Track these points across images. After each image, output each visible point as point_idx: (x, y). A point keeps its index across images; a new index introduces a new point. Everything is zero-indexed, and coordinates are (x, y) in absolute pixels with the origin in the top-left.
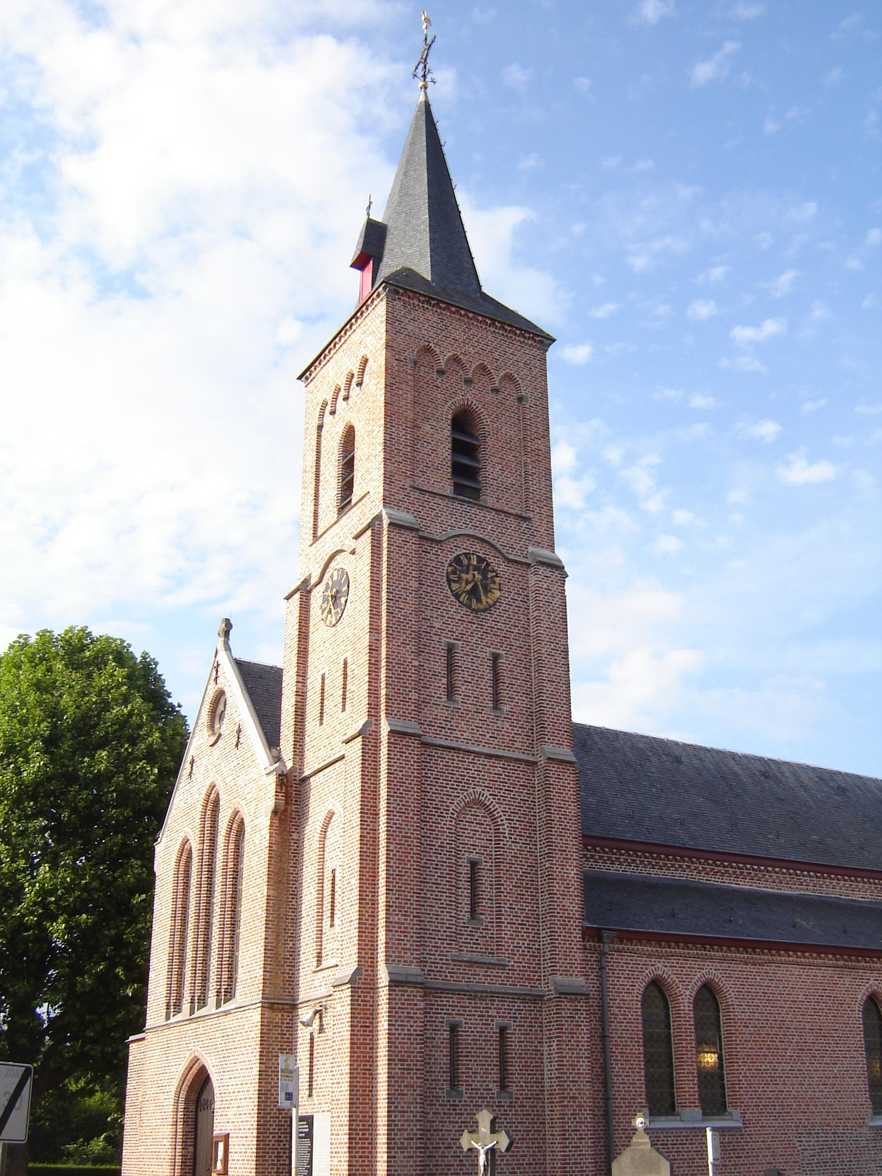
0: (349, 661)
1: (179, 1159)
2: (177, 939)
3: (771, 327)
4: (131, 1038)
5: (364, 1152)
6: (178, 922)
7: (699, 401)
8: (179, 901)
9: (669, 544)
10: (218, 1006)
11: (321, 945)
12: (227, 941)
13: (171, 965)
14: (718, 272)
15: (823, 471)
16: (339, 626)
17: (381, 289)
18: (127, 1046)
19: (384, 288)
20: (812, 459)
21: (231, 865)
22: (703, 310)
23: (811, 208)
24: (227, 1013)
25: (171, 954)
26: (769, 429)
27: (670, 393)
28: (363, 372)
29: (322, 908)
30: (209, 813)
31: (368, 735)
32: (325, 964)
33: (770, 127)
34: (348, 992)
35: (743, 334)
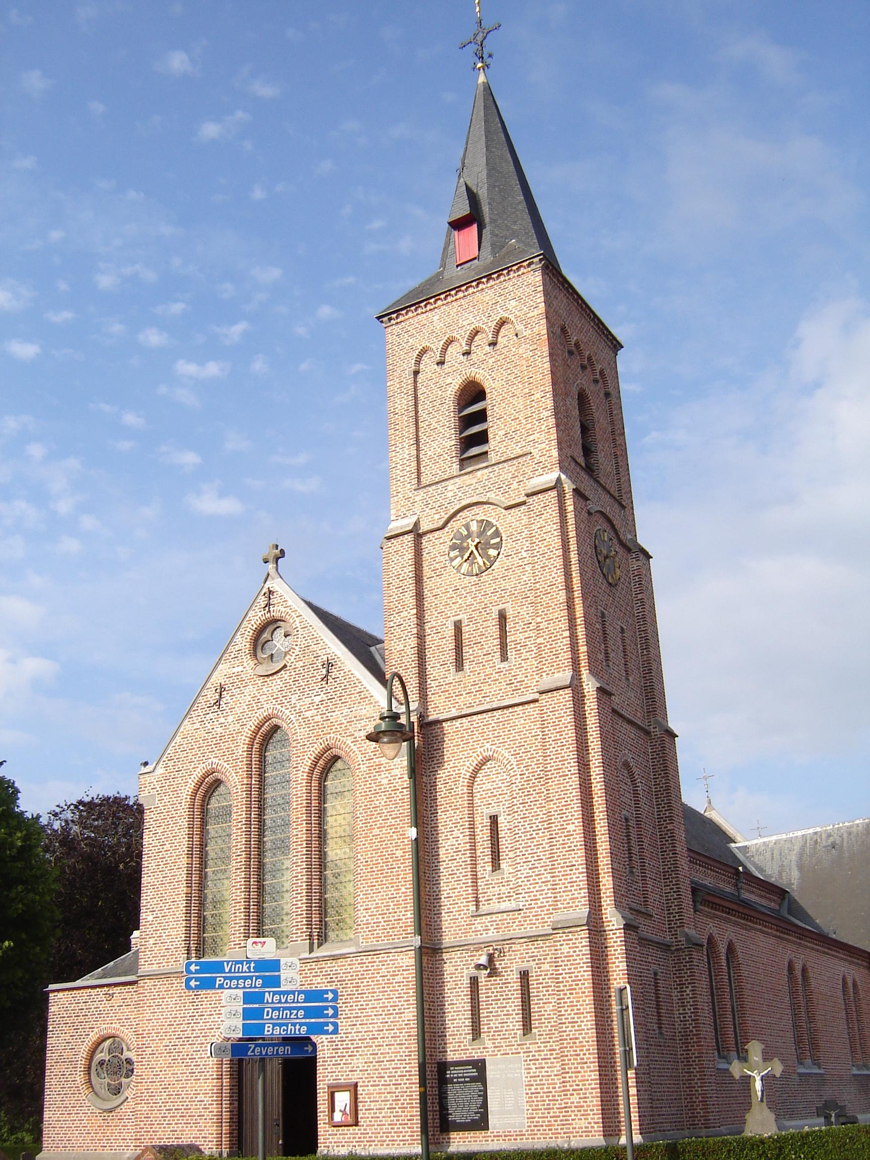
0: (510, 613)
1: (226, 1115)
2: (195, 878)
3: (213, 369)
4: (52, 987)
5: (566, 1095)
6: (196, 861)
7: (130, 419)
8: (196, 838)
9: (71, 545)
10: (311, 950)
11: (477, 890)
12: (315, 882)
13: (188, 906)
14: (178, 308)
15: (229, 506)
16: (484, 577)
17: (537, 259)
18: (46, 1000)
19: (541, 260)
20: (222, 494)
21: (315, 803)
22: (153, 338)
23: (274, 274)
24: (317, 960)
25: (189, 895)
26: (190, 458)
27: (106, 408)
28: (498, 333)
29: (475, 853)
30: (256, 746)
31: (575, 685)
32: (484, 908)
33: (258, 194)
34: (585, 934)
35: (186, 368)
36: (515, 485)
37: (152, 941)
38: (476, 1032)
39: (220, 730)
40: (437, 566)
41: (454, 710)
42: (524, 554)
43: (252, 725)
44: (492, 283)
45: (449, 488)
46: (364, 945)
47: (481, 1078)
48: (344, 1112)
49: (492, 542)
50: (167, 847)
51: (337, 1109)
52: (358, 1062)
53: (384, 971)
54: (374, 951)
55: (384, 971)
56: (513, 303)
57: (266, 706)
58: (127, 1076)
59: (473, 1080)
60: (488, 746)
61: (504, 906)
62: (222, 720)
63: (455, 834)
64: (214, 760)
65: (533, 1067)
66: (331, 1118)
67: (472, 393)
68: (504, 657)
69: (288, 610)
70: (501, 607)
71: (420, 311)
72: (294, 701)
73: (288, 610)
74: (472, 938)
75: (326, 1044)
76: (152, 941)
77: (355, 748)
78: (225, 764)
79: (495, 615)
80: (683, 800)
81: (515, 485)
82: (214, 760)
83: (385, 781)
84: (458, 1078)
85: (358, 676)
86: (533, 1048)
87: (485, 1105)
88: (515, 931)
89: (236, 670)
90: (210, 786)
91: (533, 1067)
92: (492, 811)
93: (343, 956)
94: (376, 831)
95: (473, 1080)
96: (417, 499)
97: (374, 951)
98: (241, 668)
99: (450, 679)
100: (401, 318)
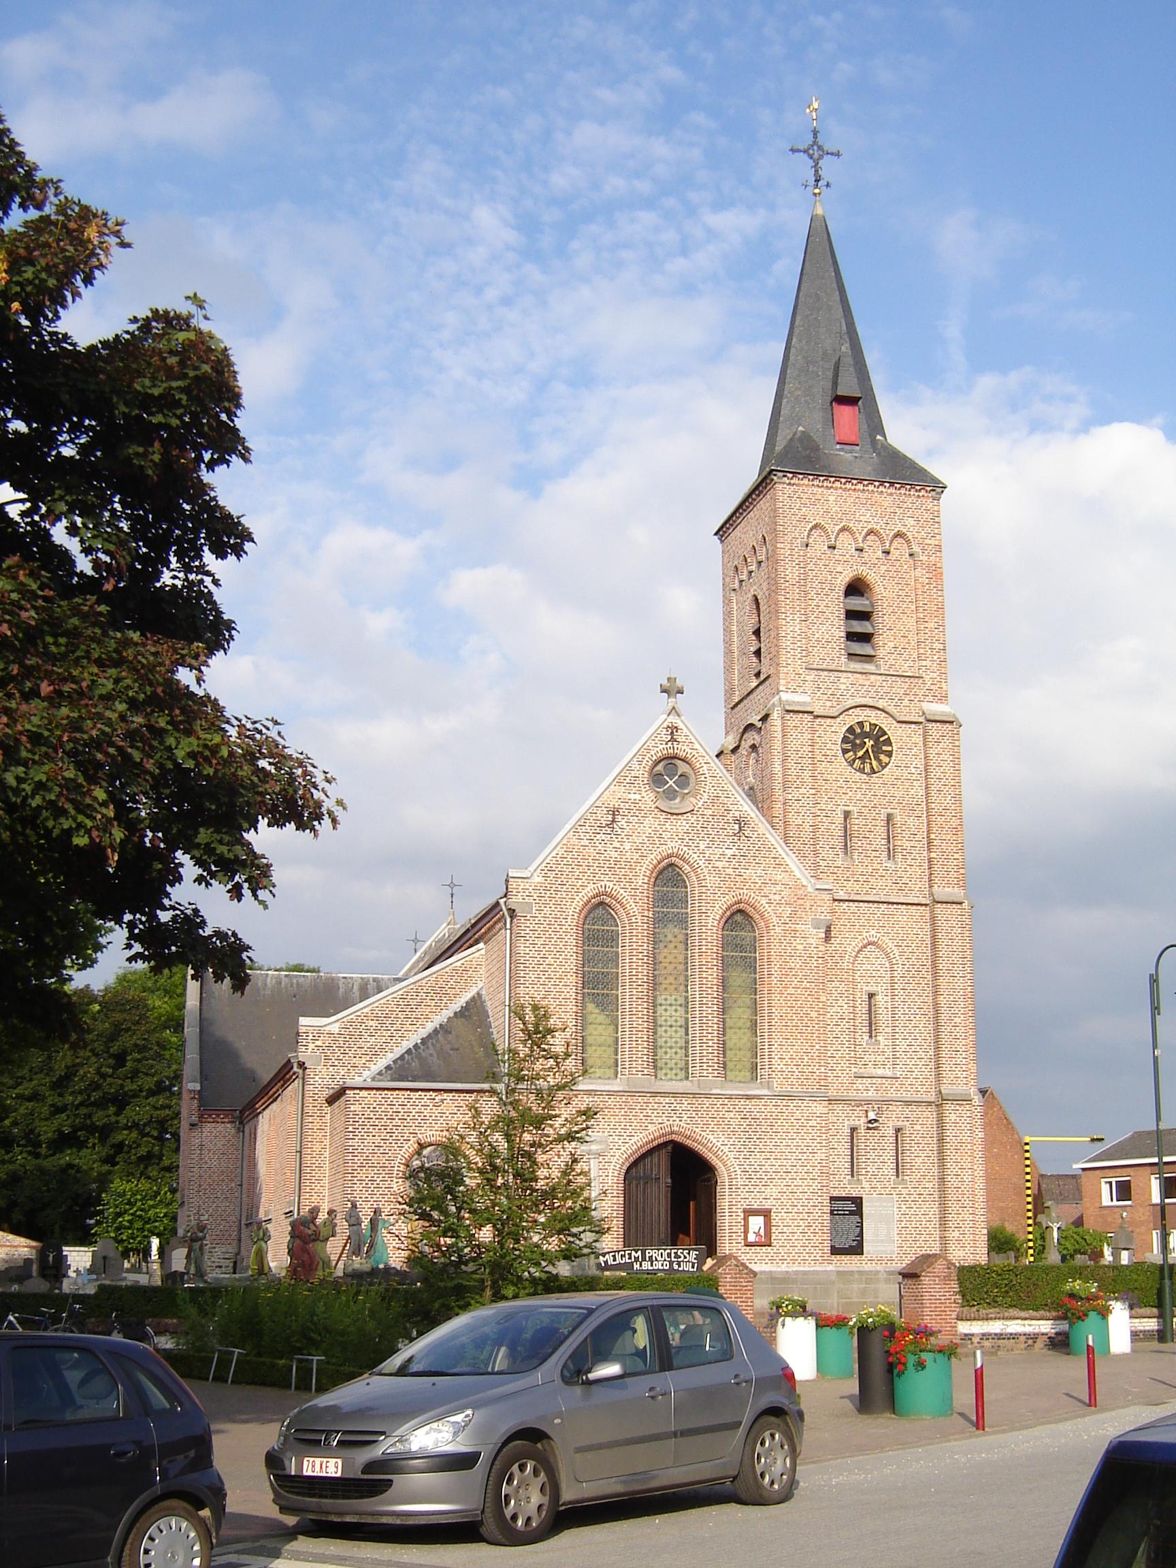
0: (898, 819)
36: (906, 702)
39: (614, 854)
41: (841, 893)
42: (913, 771)
43: (653, 858)
44: (892, 490)
45: (842, 680)
46: (777, 1089)
47: (859, 1212)
48: (757, 1234)
50: (550, 960)
51: (751, 1231)
52: (772, 1191)
53: (798, 1114)
54: (791, 1097)
55: (798, 1114)
56: (912, 522)
57: (670, 844)
61: (880, 1072)
62: (617, 844)
64: (608, 884)
66: (746, 1238)
68: (891, 854)
69: (694, 752)
70: (889, 811)
71: (816, 483)
72: (702, 847)
73: (694, 752)
74: (852, 1094)
75: (739, 1172)
77: (769, 910)
78: (622, 891)
79: (884, 817)
81: (906, 702)
82: (608, 884)
83: (799, 947)
85: (773, 842)
86: (904, 1191)
87: (861, 1234)
88: (892, 1094)
89: (633, 797)
90: (599, 911)
92: (871, 989)
93: (758, 1097)
95: (852, 1213)
96: (807, 678)
97: (791, 1097)
98: (638, 797)
99: (839, 863)
100: (795, 481)
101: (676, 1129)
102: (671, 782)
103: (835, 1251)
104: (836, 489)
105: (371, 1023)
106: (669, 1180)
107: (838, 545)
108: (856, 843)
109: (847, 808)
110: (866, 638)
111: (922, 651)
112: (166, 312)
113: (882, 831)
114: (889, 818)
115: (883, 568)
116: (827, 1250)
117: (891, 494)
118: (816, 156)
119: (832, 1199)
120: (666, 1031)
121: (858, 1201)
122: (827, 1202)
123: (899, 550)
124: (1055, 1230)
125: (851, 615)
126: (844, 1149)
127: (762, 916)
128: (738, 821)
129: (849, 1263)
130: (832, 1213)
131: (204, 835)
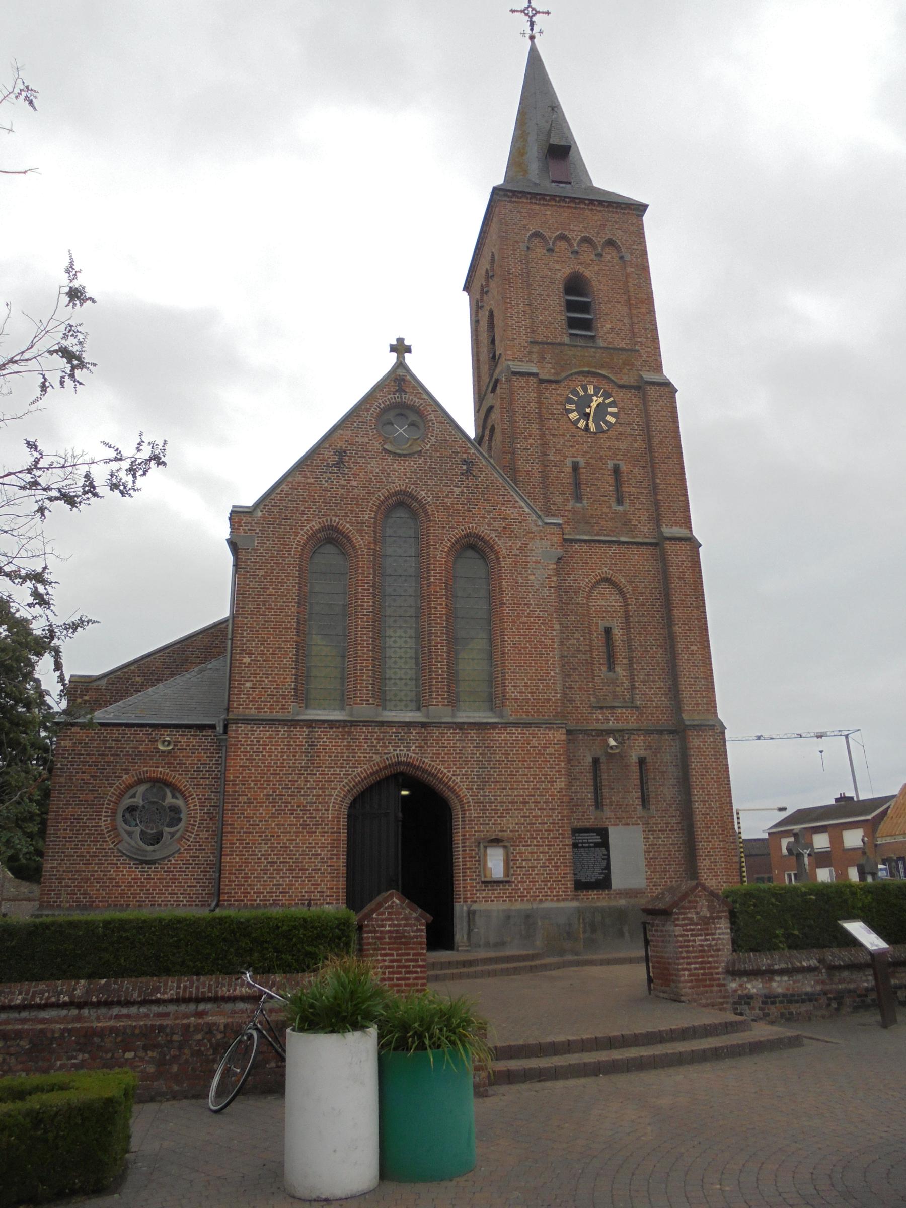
37: (248, 684)
38: (598, 804)
40: (555, 411)
47: (604, 844)
49: (610, 410)
53: (535, 743)
58: (170, 825)
59: (597, 845)
60: (605, 569)
62: (342, 482)
63: (577, 635)
65: (651, 837)
67: (575, 286)
73: (422, 401)
75: (472, 804)
76: (248, 684)
77: (499, 542)
78: (348, 526)
80: (226, 613)
84: (583, 843)
87: (608, 867)
89: (360, 440)
91: (651, 837)
94: (523, 619)
95: (597, 845)
101: (403, 759)
102: (401, 431)
103: (581, 886)
104: (552, 206)
105: (138, 679)
106: (400, 815)
107: (557, 250)
108: (586, 490)
109: (575, 459)
110: (586, 325)
111: (591, 685)
112: (625, 890)
113: (611, 479)
114: (616, 470)
115: (596, 268)
116: (570, 885)
117: (600, 211)
118: (530, 9)
119: (576, 831)
120: (395, 663)
121: (604, 833)
122: (568, 833)
123: (609, 255)
124: (806, 855)
125: (571, 306)
126: (588, 778)
127: (492, 547)
128: (464, 461)
129: (597, 900)
130: (575, 845)
131: (866, 981)
